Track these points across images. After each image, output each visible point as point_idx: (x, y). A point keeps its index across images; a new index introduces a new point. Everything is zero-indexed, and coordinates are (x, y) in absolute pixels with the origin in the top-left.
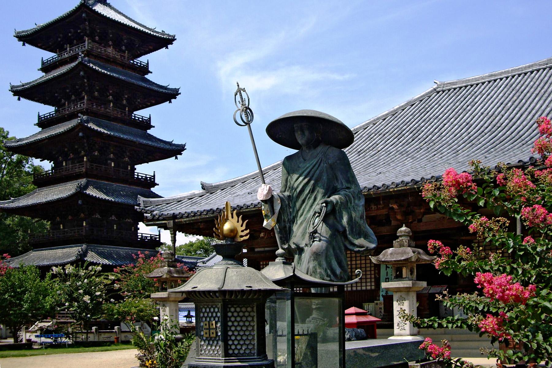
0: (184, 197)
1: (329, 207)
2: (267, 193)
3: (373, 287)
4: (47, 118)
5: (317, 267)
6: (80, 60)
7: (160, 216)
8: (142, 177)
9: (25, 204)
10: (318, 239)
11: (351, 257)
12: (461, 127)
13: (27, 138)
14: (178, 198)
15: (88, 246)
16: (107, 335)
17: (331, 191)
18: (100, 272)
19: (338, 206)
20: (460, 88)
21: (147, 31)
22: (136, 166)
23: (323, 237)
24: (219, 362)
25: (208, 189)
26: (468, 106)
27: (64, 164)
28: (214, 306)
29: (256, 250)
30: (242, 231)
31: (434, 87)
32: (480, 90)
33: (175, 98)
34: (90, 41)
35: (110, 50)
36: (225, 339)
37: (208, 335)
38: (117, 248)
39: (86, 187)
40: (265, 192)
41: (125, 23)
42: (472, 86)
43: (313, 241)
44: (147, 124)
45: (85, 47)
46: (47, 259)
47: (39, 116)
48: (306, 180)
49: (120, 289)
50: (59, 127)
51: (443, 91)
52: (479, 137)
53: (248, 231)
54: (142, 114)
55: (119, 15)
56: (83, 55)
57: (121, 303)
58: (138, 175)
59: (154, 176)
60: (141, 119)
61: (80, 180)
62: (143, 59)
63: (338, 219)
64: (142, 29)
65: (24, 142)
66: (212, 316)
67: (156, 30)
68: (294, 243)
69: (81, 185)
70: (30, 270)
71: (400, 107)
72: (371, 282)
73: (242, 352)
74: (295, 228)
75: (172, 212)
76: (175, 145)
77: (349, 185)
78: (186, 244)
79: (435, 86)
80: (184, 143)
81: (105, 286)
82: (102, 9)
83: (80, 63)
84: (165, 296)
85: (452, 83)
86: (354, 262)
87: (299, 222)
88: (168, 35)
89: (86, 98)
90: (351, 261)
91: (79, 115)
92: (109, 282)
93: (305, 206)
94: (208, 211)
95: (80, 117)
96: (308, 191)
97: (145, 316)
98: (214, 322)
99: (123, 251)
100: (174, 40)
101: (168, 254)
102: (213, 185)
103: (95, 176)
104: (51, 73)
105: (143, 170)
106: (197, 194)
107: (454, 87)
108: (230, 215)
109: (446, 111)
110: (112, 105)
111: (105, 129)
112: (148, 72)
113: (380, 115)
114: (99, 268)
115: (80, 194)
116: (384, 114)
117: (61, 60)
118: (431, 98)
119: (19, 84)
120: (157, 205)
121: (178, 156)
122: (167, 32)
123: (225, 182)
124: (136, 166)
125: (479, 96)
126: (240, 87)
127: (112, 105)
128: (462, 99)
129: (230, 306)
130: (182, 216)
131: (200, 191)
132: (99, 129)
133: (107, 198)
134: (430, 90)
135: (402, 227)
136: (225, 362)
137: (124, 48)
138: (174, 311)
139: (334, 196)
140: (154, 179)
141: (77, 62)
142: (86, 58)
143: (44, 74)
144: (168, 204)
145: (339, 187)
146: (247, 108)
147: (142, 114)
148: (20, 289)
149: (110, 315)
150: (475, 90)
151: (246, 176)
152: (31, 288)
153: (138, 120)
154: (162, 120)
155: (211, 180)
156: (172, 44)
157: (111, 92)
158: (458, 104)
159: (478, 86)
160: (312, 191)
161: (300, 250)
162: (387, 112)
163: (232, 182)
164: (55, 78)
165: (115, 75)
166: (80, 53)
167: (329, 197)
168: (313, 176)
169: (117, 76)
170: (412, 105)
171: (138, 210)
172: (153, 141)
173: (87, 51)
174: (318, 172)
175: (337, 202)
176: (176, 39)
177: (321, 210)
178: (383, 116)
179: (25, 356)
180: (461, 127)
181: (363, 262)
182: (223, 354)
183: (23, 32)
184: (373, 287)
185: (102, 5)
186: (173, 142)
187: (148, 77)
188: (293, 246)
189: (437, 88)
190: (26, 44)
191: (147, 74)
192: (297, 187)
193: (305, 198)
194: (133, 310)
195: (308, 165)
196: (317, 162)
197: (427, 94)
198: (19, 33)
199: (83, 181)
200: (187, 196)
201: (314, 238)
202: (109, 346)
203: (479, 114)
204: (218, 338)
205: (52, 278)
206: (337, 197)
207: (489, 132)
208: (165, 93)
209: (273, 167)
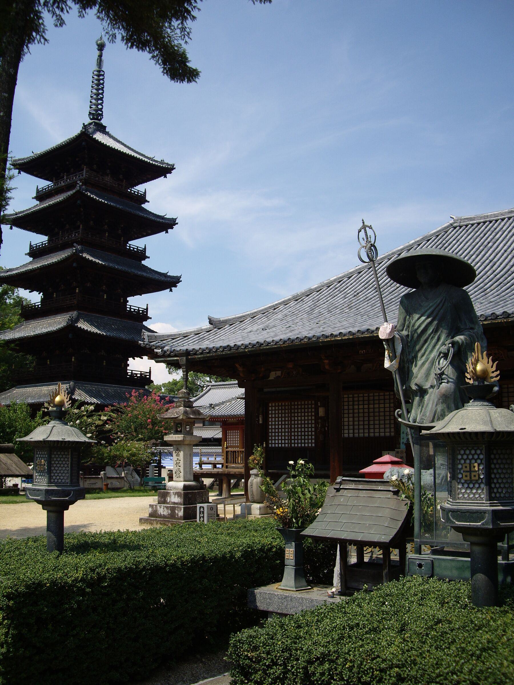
0: (191, 332)
1: (456, 347)
2: (391, 332)
3: (393, 434)
4: (39, 248)
5: (446, 410)
6: (78, 188)
7: (171, 352)
8: (134, 310)
9: (11, 337)
10: (446, 381)
11: (369, 400)
12: (485, 264)
13: (17, 269)
14: (185, 333)
15: (75, 383)
16: (92, 481)
17: (453, 332)
18: (92, 411)
19: (464, 347)
20: (479, 224)
21: (146, 160)
22: (128, 299)
23: (450, 378)
24: (483, 506)
25: (216, 324)
26: (489, 243)
27: (55, 295)
28: (476, 448)
29: (266, 390)
30: (493, 372)
31: (451, 222)
32: (500, 226)
33: (172, 228)
34: (88, 169)
35: (108, 179)
36: (489, 481)
37: (468, 478)
38: (105, 386)
39: (77, 320)
40: (388, 331)
41: (124, 152)
42: (491, 222)
43: (442, 383)
44: (142, 255)
45: (83, 175)
46: (31, 397)
47: (31, 246)
48: (430, 319)
49: (111, 431)
50: (51, 257)
51: (461, 227)
52: (506, 276)
53: (498, 372)
54: (137, 244)
55: (118, 144)
56: (81, 184)
57: (112, 446)
58: (130, 308)
59: (147, 309)
60: (135, 250)
61: (71, 313)
62: (140, 188)
63: (464, 360)
64: (141, 157)
65: (14, 272)
66: (473, 458)
67: (155, 159)
68: (416, 384)
69: (72, 317)
70: (20, 408)
71: (415, 242)
72: (390, 428)
73: (502, 495)
74: (415, 370)
75: (185, 348)
76: (170, 276)
77: (472, 326)
78: (169, 382)
79: (452, 221)
80: (179, 275)
81: (96, 427)
82: (101, 137)
83: (78, 192)
84: (179, 439)
85: (471, 218)
87: (420, 363)
88: (167, 164)
89: (81, 227)
90: (369, 404)
91: (75, 244)
92: (100, 423)
93: (428, 346)
94: (225, 348)
95: (75, 247)
96: (431, 331)
97: (137, 461)
98: (476, 465)
99: (111, 389)
101: (185, 393)
102: (221, 319)
103: (87, 310)
104: (46, 202)
105: (136, 302)
106: (204, 329)
107: (471, 222)
108: (480, 355)
109: (465, 247)
110: (107, 234)
111: (99, 260)
113: (394, 250)
114: (92, 408)
115: (71, 328)
116: (399, 248)
117: (57, 188)
118: (448, 233)
119: (13, 212)
120: (162, 341)
121: (173, 288)
122: (166, 161)
123: (234, 316)
124: (128, 299)
125: (500, 233)
126: (365, 224)
127: (107, 234)
128: (482, 235)
129: (459, 449)
130: (195, 352)
131: (206, 325)
132: (94, 260)
133: (99, 332)
134: (446, 225)
136: (491, 506)
137: (121, 176)
138: (189, 456)
139: (459, 337)
140: (147, 312)
141: (74, 191)
142: (84, 187)
143: (38, 202)
144: (173, 339)
145: (462, 327)
146: (373, 245)
147: (137, 244)
148: (10, 429)
149: (99, 458)
150: (495, 227)
151: (256, 310)
152: (21, 428)
153: (133, 250)
155: (220, 315)
156: (171, 173)
157: (107, 221)
158: (478, 240)
159: (498, 222)
160: (435, 331)
161: (422, 392)
162: (402, 247)
163: (241, 317)
164: (50, 206)
165: (112, 204)
166: (78, 182)
167: (452, 338)
168: (436, 316)
169: (115, 205)
170: (428, 241)
171: (142, 345)
172: (147, 273)
173: (85, 179)
174: (442, 311)
175: (463, 342)
176: (175, 168)
177: (449, 351)
178: (398, 251)
179: (16, 502)
180: (485, 264)
182: (488, 497)
183: (19, 160)
184: (393, 434)
185: (101, 134)
186: (168, 274)
187: (145, 206)
188: (414, 387)
189: (454, 223)
190: (22, 172)
191: (144, 203)
192: (419, 326)
193: (428, 338)
194: (125, 454)
195: (431, 305)
196: (441, 301)
197: (443, 229)
198: (15, 161)
199: (75, 314)
200: (194, 331)
201: (442, 379)
202: (98, 493)
203: (502, 251)
204: (480, 481)
205: (43, 418)
206: (462, 337)
208: (162, 223)
209: (284, 302)
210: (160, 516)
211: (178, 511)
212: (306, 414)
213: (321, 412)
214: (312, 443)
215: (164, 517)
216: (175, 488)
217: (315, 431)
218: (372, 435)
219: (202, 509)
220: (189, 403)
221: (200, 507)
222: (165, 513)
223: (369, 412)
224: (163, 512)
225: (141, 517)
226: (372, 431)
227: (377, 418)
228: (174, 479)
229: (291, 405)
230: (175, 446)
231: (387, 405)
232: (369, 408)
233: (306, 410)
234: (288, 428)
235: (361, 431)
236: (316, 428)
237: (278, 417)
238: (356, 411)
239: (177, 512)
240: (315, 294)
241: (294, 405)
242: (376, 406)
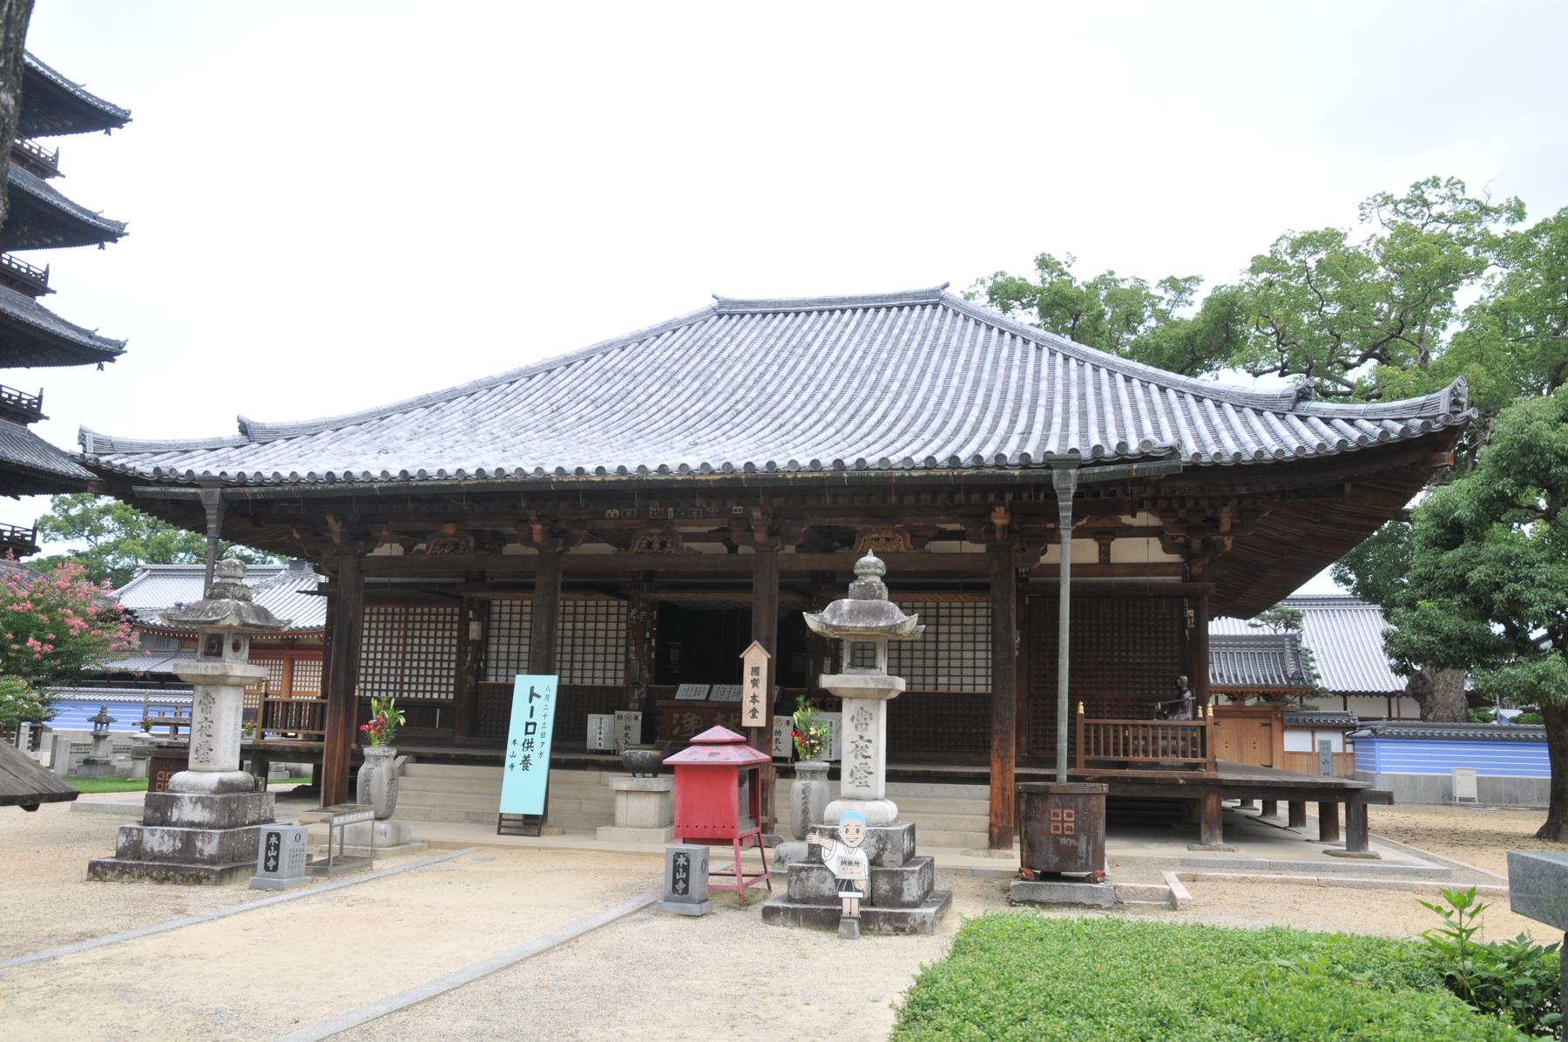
3: (620, 682)
11: (575, 614)
44: (35, 285)
80: (122, 339)
86: (580, 626)
90: (574, 622)
100: (126, 121)
112: (55, 173)
121: (106, 364)
131: (233, 432)
135: (865, 554)
154: (72, 285)
155: (260, 416)
181: (602, 626)
184: (620, 682)
207: (887, 387)
210: (155, 857)
212: (432, 633)
213: (475, 630)
214: (447, 692)
215: (161, 856)
216: (193, 788)
217: (457, 669)
218: (577, 682)
219: (274, 840)
220: (243, 591)
221: (270, 835)
223: (573, 637)
225: (94, 859)
226: (588, 674)
227: (590, 649)
228: (191, 766)
229: (407, 614)
230: (199, 688)
231: (613, 626)
232: (574, 630)
233: (440, 626)
234: (397, 660)
235: (599, 674)
236: (460, 662)
237: (377, 637)
238: (579, 633)
239: (199, 844)
240: (420, 413)
241: (415, 614)
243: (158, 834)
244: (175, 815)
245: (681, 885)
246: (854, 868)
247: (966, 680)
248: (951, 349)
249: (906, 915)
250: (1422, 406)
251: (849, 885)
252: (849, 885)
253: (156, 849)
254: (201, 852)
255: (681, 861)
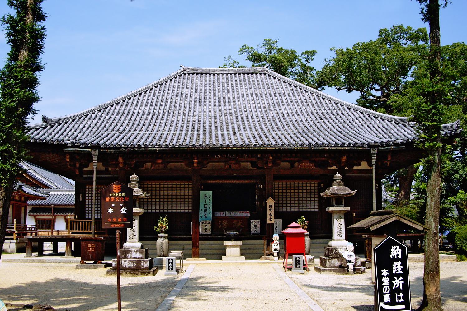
79: (182, 69)
102: (52, 119)
211: (143, 263)
221: (296, 258)
222: (130, 266)
224: (128, 265)
239: (142, 264)
242: (292, 191)
243: (127, 261)
244: (129, 256)
245: (298, 265)
246: (351, 257)
247: (308, 207)
248: (259, 115)
249: (360, 269)
250: (448, 127)
251: (350, 262)
252: (350, 262)
253: (127, 266)
254: (143, 266)
255: (298, 259)
